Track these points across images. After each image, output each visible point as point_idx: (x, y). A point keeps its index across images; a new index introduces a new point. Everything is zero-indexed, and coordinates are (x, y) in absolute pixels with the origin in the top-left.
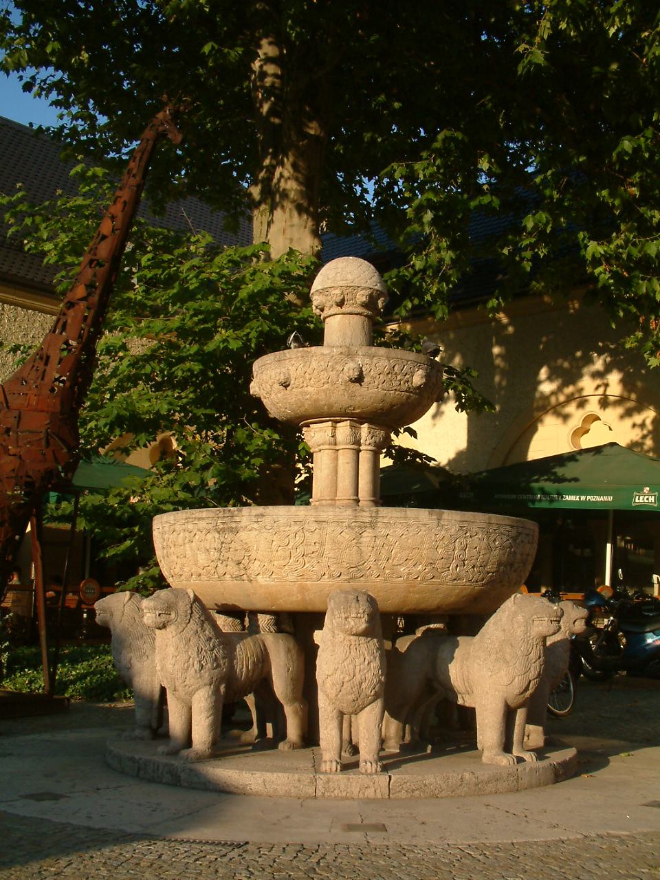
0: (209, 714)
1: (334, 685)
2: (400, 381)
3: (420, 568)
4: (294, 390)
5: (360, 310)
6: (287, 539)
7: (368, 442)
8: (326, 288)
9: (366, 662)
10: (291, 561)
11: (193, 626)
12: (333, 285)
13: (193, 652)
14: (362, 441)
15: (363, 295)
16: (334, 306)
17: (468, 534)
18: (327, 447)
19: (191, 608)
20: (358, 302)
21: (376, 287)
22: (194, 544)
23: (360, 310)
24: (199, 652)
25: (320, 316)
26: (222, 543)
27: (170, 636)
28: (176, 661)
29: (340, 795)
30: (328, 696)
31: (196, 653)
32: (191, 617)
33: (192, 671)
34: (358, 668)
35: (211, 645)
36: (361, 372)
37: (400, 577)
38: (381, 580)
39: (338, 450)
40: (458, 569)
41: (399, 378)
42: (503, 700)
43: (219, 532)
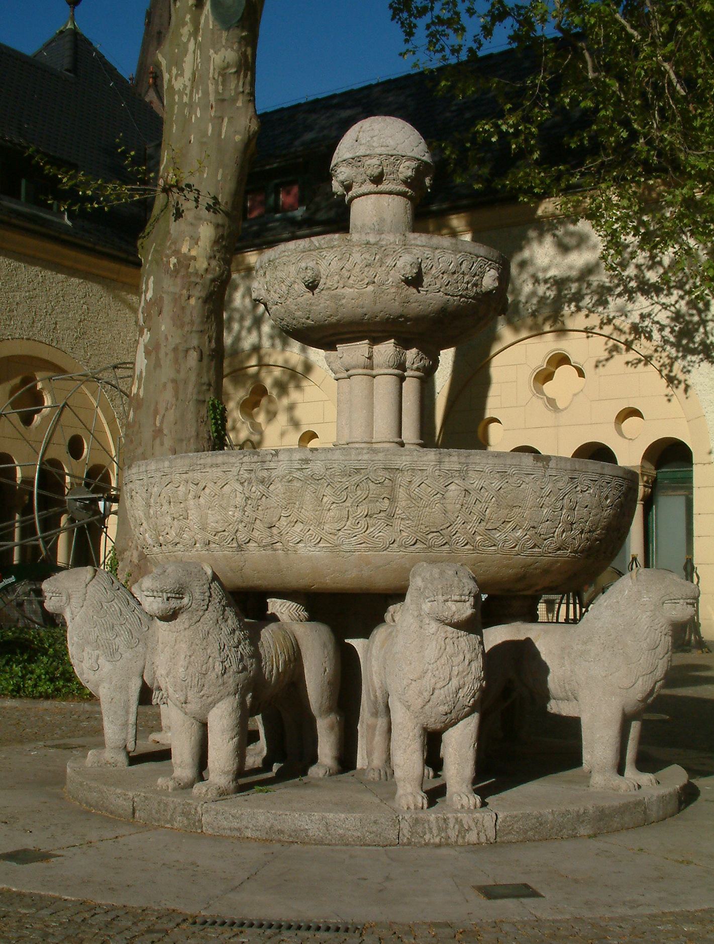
0: (234, 733)
1: (421, 693)
2: (468, 283)
3: (519, 533)
4: (323, 292)
5: (403, 188)
6: (344, 493)
7: (415, 366)
8: (358, 157)
9: (467, 662)
10: (348, 523)
11: (211, 615)
12: (368, 152)
13: (213, 650)
14: (408, 364)
15: (409, 168)
16: (368, 181)
17: (578, 489)
18: (361, 371)
19: (210, 588)
20: (401, 177)
21: (424, 158)
22: (202, 500)
23: (403, 188)
24: (221, 650)
25: (344, 196)
26: (247, 498)
27: (182, 627)
28: (189, 663)
29: (432, 841)
30: (408, 707)
31: (218, 652)
32: (210, 601)
33: (212, 676)
34: (456, 669)
35: (236, 640)
36: (420, 269)
37: (494, 545)
38: (469, 550)
39: (374, 377)
40: (564, 536)
41: (466, 279)
42: (621, 709)
43: (242, 484)
